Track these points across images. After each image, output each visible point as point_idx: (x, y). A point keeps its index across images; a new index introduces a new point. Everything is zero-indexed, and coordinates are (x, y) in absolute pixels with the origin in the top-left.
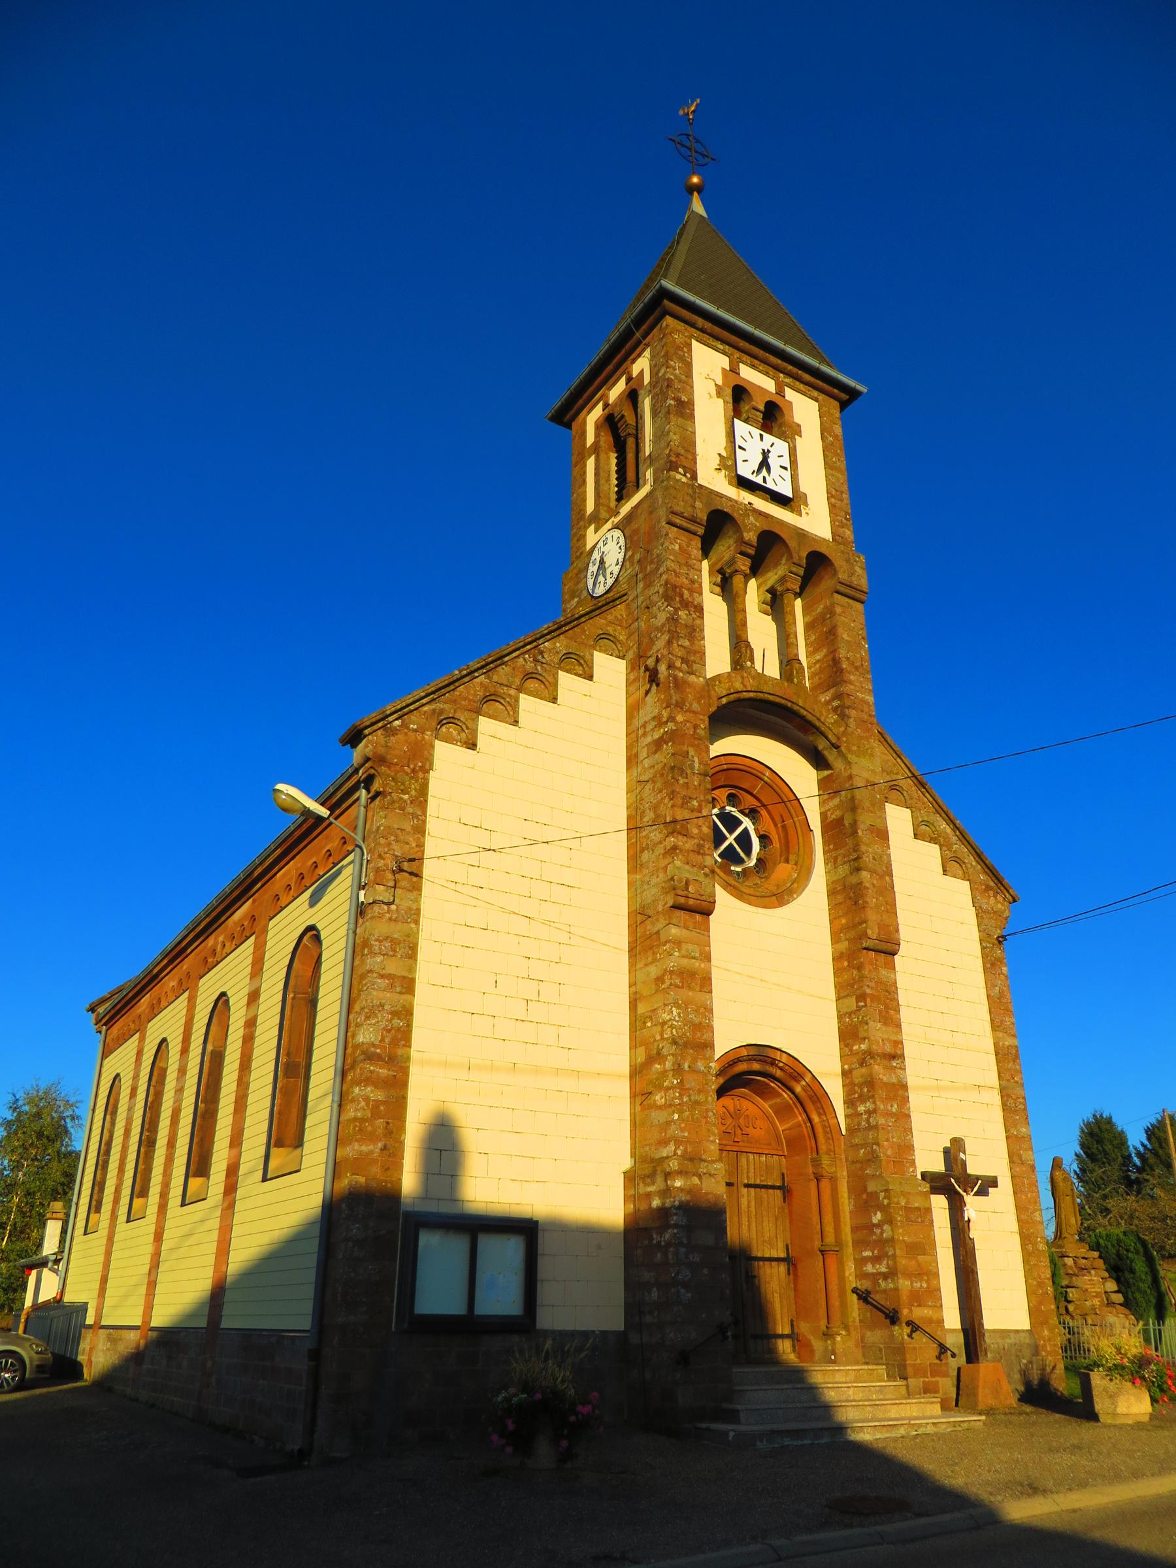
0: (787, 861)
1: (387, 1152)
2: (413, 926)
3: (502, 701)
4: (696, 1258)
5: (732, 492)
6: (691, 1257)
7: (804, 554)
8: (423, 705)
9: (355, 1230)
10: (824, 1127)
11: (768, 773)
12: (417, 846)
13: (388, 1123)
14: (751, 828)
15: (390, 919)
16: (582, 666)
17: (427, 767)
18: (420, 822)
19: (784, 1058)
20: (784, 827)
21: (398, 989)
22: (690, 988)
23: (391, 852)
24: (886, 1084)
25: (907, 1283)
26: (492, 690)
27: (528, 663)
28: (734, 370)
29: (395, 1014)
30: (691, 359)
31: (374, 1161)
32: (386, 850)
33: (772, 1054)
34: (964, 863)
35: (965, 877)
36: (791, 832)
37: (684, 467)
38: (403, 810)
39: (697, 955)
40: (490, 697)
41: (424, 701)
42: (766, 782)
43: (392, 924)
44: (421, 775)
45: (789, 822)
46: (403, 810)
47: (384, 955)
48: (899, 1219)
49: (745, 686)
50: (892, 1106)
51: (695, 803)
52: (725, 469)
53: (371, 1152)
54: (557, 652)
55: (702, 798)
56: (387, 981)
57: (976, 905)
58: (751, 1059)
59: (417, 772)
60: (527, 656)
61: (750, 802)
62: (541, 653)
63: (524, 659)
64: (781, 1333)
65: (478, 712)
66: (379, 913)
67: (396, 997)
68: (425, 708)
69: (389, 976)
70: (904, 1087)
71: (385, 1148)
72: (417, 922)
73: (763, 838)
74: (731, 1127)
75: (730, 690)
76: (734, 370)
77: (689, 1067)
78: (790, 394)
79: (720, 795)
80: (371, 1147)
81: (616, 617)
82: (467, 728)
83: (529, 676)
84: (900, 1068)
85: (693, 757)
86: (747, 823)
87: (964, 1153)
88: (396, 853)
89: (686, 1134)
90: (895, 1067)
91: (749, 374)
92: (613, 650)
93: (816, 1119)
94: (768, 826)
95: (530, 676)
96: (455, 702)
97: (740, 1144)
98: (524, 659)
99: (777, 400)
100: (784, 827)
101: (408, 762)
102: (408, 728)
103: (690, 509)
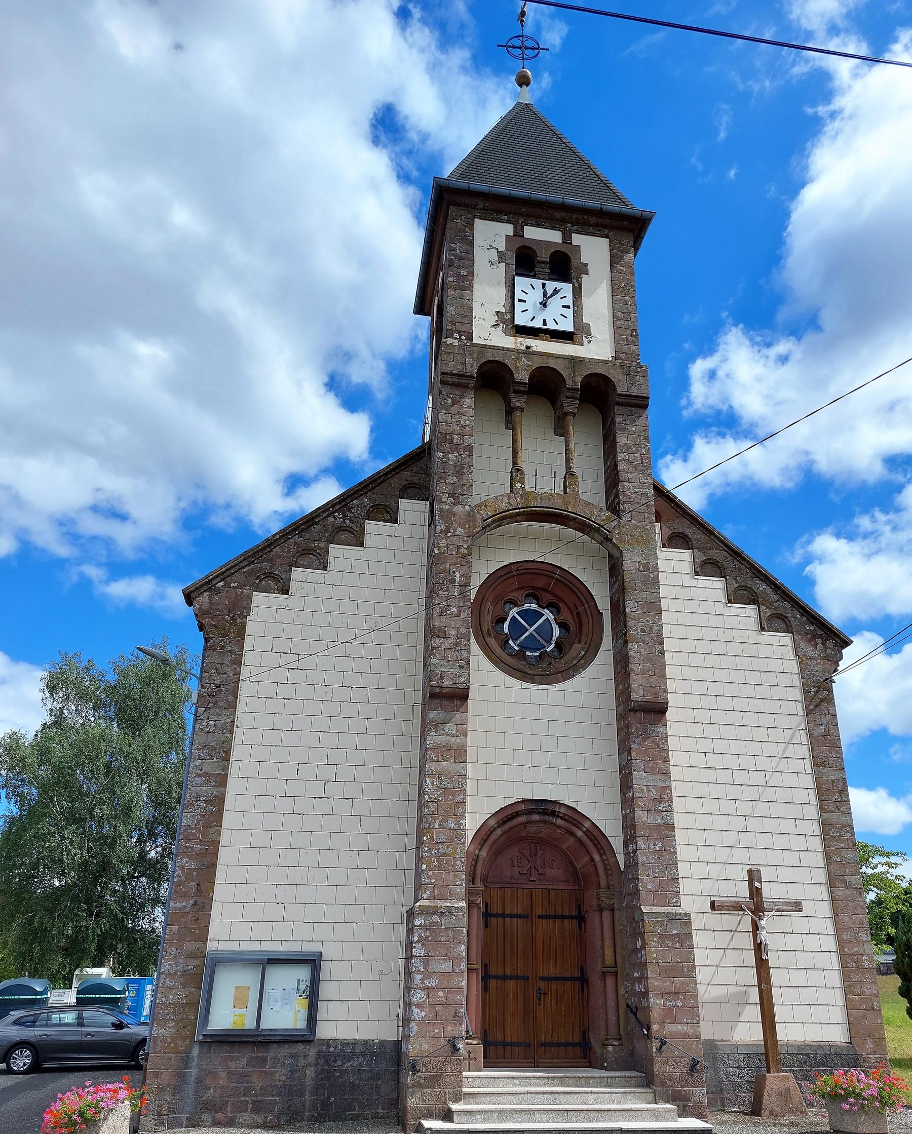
0: (579, 642)
1: (197, 907)
2: (228, 735)
3: (314, 553)
4: (432, 983)
5: (510, 342)
6: (426, 982)
7: (579, 379)
8: (243, 567)
9: (167, 966)
10: (605, 865)
11: (558, 572)
12: (233, 675)
13: (199, 885)
14: (551, 617)
15: (208, 732)
16: (389, 513)
17: (245, 614)
18: (237, 656)
19: (563, 810)
20: (578, 613)
21: (212, 784)
22: (445, 760)
23: (212, 682)
24: (650, 827)
25: (660, 1002)
26: (304, 546)
27: (338, 519)
28: (518, 233)
29: (209, 802)
30: (473, 237)
31: (187, 914)
32: (207, 681)
33: (550, 807)
34: (786, 617)
35: (788, 630)
36: (583, 616)
37: (459, 332)
38: (223, 650)
39: (454, 732)
40: (307, 552)
41: (243, 564)
42: (557, 579)
43: (210, 735)
44: (239, 620)
45: (581, 609)
46: (223, 650)
47: (202, 759)
48: (653, 944)
49: (511, 505)
50: (655, 845)
51: (454, 610)
52: (503, 323)
53: (185, 907)
54: (365, 506)
55: (461, 605)
56: (204, 779)
57: (799, 654)
58: (530, 812)
59: (236, 619)
60: (337, 514)
61: (548, 598)
62: (350, 510)
63: (334, 517)
64: (509, 1041)
65: (291, 565)
66: (199, 728)
67: (211, 789)
68: (245, 569)
69: (206, 775)
70: (671, 827)
71: (195, 904)
72: (231, 732)
73: (562, 625)
74: (526, 869)
75: (496, 511)
76: (518, 233)
77: (439, 825)
78: (577, 239)
79: (518, 596)
80: (184, 904)
81: (421, 468)
82: (282, 579)
83: (341, 529)
84: (667, 811)
85: (454, 573)
86: (548, 614)
87: (760, 882)
88: (215, 682)
89: (433, 881)
90: (662, 811)
91: (532, 233)
92: (420, 494)
93: (597, 858)
94: (566, 616)
95: (340, 529)
96: (271, 560)
97: (537, 882)
98: (334, 517)
99: (564, 249)
100: (578, 613)
101: (229, 612)
102: (230, 587)
103: (460, 367)
